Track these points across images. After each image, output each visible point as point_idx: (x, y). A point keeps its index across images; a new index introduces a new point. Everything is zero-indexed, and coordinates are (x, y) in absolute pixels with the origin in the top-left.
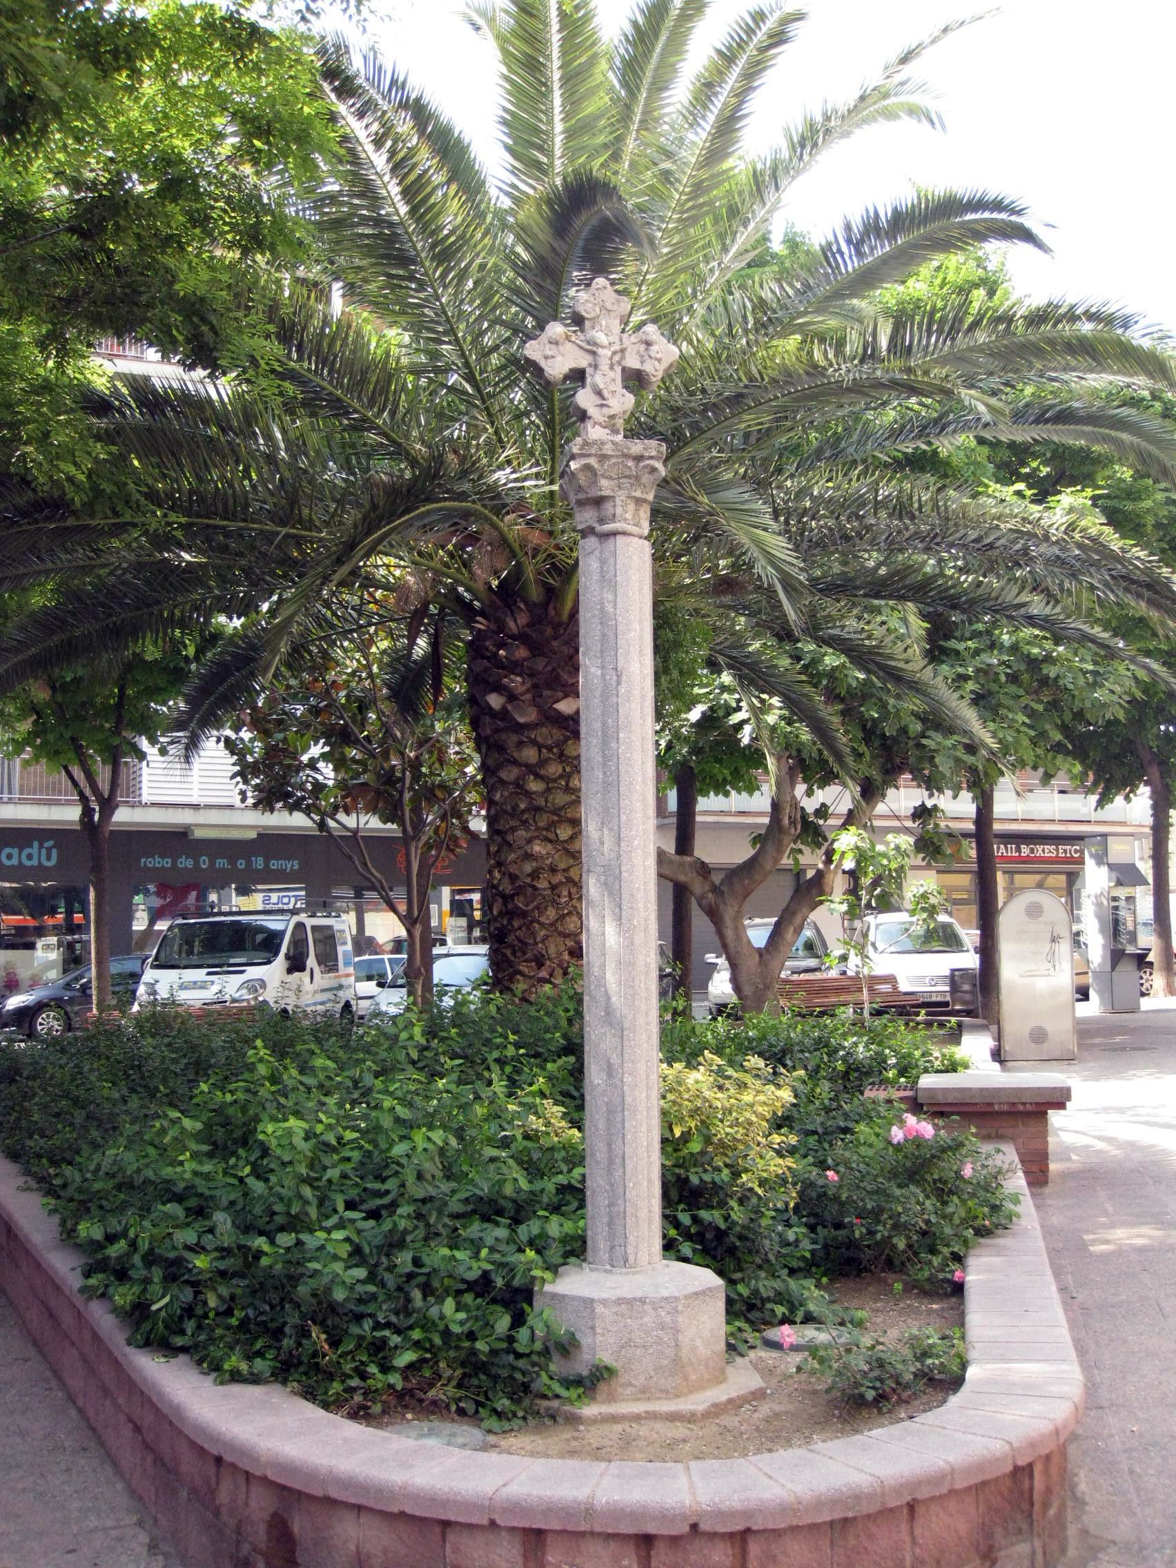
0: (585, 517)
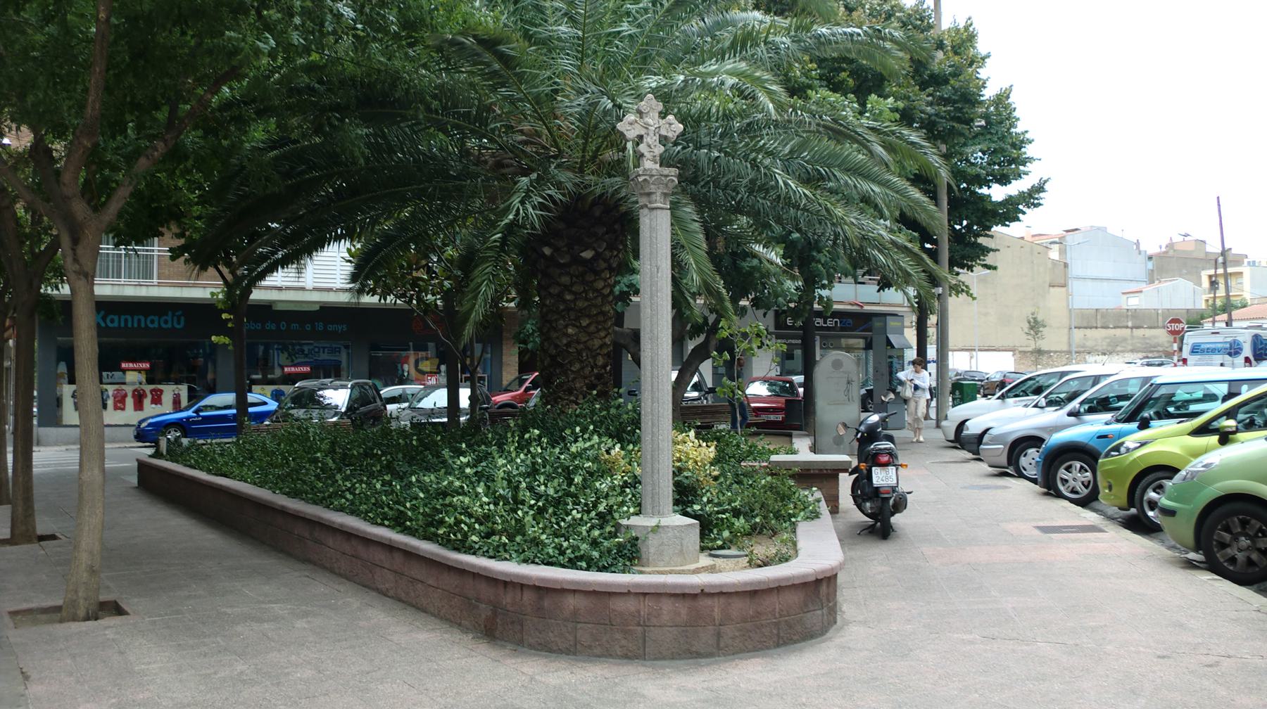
0: (643, 201)
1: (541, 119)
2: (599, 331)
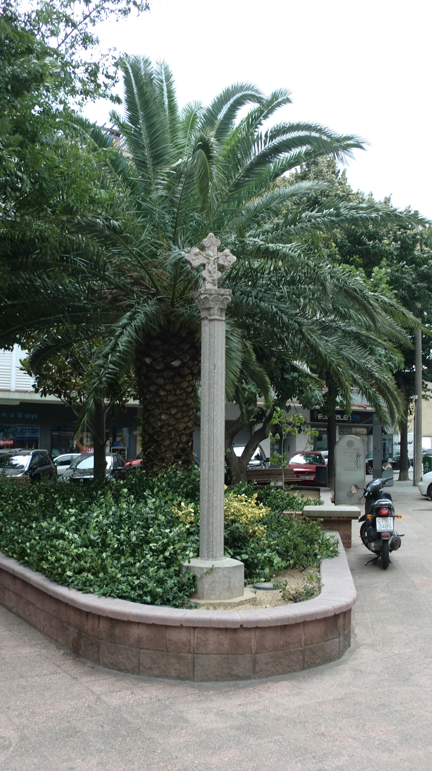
1: (143, 268)
2: (183, 417)
